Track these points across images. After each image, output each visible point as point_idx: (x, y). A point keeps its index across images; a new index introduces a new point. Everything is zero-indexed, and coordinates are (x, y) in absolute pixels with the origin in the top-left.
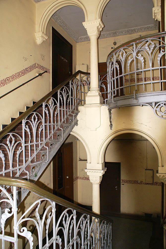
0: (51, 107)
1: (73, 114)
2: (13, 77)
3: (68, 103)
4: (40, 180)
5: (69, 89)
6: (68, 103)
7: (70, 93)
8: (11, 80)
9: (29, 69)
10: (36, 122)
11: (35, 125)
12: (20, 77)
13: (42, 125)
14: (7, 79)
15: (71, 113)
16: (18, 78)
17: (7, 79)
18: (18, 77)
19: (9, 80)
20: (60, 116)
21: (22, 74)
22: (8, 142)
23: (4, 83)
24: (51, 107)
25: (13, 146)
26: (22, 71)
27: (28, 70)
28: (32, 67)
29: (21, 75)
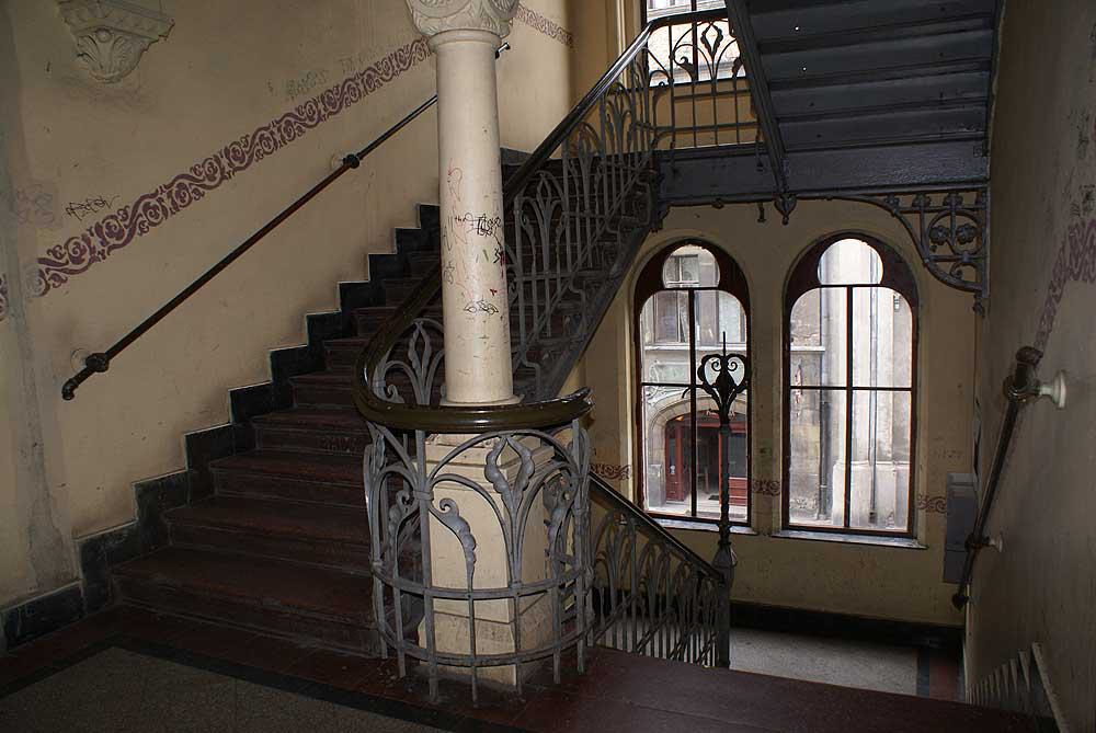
0: (414, 371)
1: (536, 365)
2: (288, 123)
3: (596, 187)
4: (733, 99)
5: (561, 182)
6: (596, 187)
7: (565, 197)
8: (225, 161)
9: (362, 81)
10: (425, 362)
11: (422, 373)
12: (320, 119)
13: (515, 284)
14: (147, 207)
15: (571, 288)
16: (311, 127)
17: (147, 207)
18: (310, 123)
19: (155, 207)
20: (573, 239)
21: (402, 66)
22: (412, 354)
23: (257, 141)
24: (414, 371)
25: (428, 368)
26: (331, 95)
27: (401, 62)
28: (375, 72)
29: (360, 81)
